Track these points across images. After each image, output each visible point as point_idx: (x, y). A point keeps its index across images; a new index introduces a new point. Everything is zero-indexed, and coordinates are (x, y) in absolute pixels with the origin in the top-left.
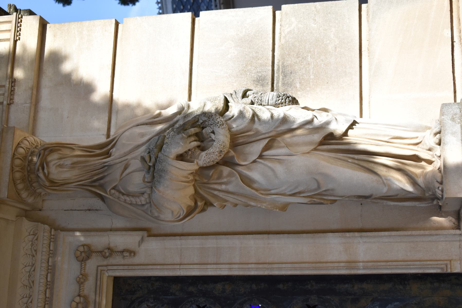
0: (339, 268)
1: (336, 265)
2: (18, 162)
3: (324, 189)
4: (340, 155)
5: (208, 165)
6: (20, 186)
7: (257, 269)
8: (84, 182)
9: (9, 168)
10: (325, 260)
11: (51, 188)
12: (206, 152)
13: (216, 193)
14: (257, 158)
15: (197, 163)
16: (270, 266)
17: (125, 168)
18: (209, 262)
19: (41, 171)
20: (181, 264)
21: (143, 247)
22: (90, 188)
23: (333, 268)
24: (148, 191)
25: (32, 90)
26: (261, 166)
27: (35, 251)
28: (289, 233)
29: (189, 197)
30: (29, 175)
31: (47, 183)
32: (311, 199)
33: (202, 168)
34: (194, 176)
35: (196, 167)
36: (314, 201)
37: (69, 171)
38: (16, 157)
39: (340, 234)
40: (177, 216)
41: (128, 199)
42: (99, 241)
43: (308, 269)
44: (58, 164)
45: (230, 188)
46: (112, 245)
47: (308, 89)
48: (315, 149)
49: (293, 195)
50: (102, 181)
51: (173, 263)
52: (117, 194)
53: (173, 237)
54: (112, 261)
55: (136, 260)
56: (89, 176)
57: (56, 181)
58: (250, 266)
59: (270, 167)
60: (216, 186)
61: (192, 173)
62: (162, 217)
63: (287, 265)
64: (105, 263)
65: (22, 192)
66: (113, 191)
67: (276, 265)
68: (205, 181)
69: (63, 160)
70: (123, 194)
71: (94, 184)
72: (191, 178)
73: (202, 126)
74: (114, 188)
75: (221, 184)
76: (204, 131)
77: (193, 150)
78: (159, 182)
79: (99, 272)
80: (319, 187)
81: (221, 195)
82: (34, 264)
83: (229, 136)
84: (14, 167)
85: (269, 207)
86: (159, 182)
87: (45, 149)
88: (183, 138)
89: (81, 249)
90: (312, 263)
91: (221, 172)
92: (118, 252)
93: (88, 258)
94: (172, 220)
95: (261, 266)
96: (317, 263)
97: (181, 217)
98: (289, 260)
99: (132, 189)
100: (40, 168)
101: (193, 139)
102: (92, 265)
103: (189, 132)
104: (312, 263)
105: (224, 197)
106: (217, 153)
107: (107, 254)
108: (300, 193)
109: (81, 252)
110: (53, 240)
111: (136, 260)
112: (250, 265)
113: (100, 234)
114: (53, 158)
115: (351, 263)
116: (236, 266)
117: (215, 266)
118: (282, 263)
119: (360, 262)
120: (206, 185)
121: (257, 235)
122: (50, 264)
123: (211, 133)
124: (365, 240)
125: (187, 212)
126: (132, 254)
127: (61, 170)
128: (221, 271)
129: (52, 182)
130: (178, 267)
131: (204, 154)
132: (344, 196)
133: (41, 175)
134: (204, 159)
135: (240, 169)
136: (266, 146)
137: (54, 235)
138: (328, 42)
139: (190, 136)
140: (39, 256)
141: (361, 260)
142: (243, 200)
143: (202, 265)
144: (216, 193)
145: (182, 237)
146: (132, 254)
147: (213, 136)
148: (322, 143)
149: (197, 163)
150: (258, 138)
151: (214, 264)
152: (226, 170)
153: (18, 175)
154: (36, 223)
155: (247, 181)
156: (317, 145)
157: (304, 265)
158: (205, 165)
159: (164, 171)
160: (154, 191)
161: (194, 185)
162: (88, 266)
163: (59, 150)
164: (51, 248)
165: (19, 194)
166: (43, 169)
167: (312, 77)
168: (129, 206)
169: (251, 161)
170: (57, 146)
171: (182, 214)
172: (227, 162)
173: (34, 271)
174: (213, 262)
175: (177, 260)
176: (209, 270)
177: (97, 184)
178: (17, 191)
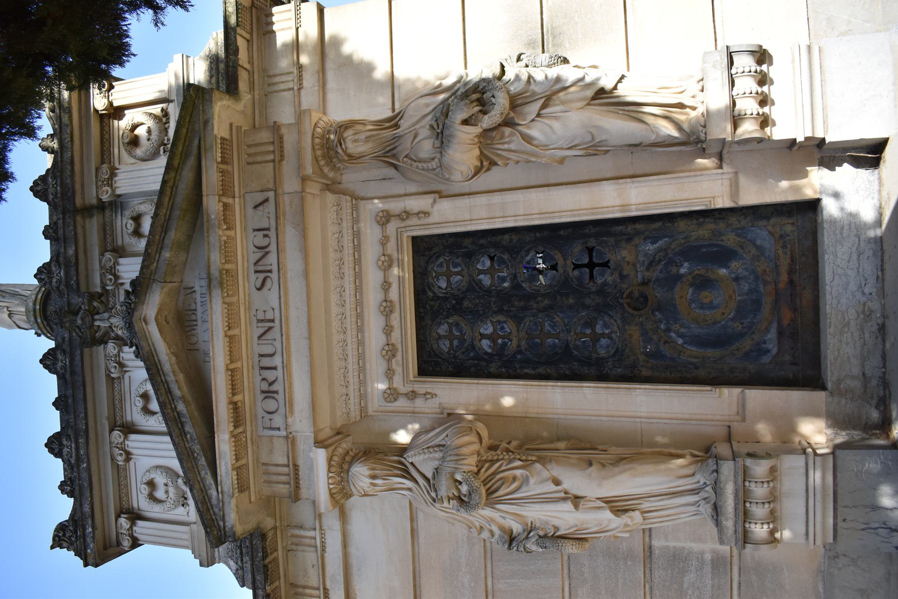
4: (611, 108)
6: (322, 163)
13: (499, 152)
17: (415, 137)
21: (436, 207)
24: (438, 155)
28: (567, 184)
33: (486, 131)
35: (480, 130)
41: (420, 165)
42: (396, 206)
43: (586, 215)
45: (512, 146)
46: (408, 209)
48: (588, 104)
50: (394, 152)
52: (409, 161)
54: (409, 222)
55: (431, 220)
59: (547, 125)
62: (453, 178)
64: (403, 225)
66: (405, 159)
68: (489, 142)
70: (415, 161)
72: (477, 140)
74: (406, 157)
75: (503, 143)
81: (504, 153)
88: (466, 104)
89: (381, 214)
91: (503, 132)
93: (388, 221)
95: (543, 216)
98: (569, 208)
99: (423, 155)
101: (475, 104)
102: (392, 228)
108: (575, 146)
110: (355, 208)
111: (431, 220)
117: (502, 219)
124: (636, 185)
131: (486, 117)
133: (340, 150)
134: (487, 121)
135: (520, 128)
139: (472, 102)
140: (344, 224)
142: (525, 156)
144: (499, 152)
147: (493, 100)
148: (594, 98)
152: (507, 131)
153: (319, 153)
155: (528, 139)
166: (341, 145)
172: (508, 123)
175: (468, 217)
177: (389, 154)
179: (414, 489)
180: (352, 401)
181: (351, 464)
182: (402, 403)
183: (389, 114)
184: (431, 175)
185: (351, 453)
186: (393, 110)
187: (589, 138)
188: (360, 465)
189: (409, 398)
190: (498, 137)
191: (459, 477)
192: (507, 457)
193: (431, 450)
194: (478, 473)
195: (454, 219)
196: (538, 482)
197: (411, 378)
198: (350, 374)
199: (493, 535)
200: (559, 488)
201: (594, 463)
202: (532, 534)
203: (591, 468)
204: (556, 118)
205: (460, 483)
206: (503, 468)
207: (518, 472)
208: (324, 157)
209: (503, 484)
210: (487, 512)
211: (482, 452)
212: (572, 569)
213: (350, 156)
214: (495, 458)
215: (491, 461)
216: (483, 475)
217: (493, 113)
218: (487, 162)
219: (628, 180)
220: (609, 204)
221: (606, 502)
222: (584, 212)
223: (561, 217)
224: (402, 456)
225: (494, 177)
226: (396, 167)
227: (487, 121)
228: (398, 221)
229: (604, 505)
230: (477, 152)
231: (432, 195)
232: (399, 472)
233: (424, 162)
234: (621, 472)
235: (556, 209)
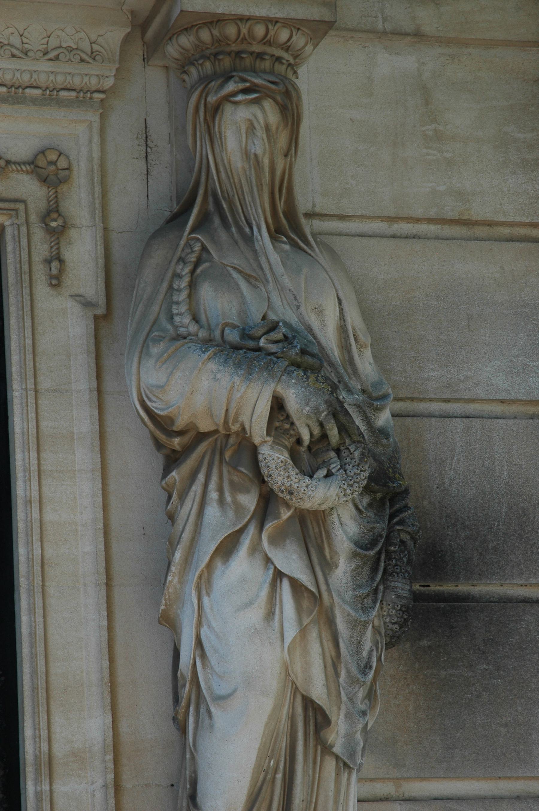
0: (37, 740)
1: (44, 733)
2: (260, 30)
3: (213, 709)
4: (284, 743)
5: (262, 464)
6: (205, 35)
7: (30, 560)
8: (215, 178)
9: (247, 13)
10: (54, 708)
11: (202, 106)
12: (290, 461)
13: (201, 477)
14: (275, 568)
15: (266, 442)
16: (38, 590)
17: (247, 278)
18: (43, 455)
19: (241, 86)
20: (36, 391)
21: (70, 304)
22: (201, 191)
23: (36, 727)
24: (203, 334)
25: (415, 35)
26: (262, 577)
27: (57, 58)
28: (110, 629)
29: (191, 422)
30: (229, 54)
31: (215, 98)
32: (189, 678)
33: (254, 450)
34: (237, 433)
35: (257, 440)
36: (184, 686)
37: (241, 146)
38: (270, 27)
39: (110, 741)
40: (151, 396)
41: (184, 283)
42: (78, 202)
43: (34, 673)
44: (256, 124)
45: (212, 511)
46: (73, 233)
47: (417, 665)
48: (296, 690)
49: (199, 643)
50: (217, 221)
51: (38, 372)
52: (193, 258)
53: (95, 374)
54: (38, 234)
55: (42, 290)
56: (229, 189)
57: (217, 122)
58: (37, 545)
59: (257, 596)
60: (214, 479)
61: (244, 429)
62: (149, 364)
63: (42, 626)
64: (33, 218)
65: (192, 38)
66: (197, 247)
67: (41, 601)
68: (227, 455)
69: (265, 136)
70: (193, 272)
71: (211, 199)
72: (235, 428)
73: (342, 448)
74: (204, 249)
75: (220, 490)
76: (333, 454)
77: (292, 432)
78: (225, 362)
79: (12, 206)
80: (220, 699)
81: (197, 488)
82: (26, 54)
83: (323, 507)
84: (249, 22)
85: (170, 590)
86: (225, 362)
87: (287, 93)
88: (317, 411)
89: (62, 163)
90: (47, 682)
91: (247, 491)
92: (58, 249)
93: (44, 180)
94: (142, 384)
95: (37, 568)
96: (47, 692)
97: (149, 403)
98: (51, 631)
99: (207, 293)
100: (248, 84)
101: (317, 431)
102: (27, 187)
103: (331, 425)
104: (47, 682)
105: (191, 494)
106: (288, 484)
107: (53, 224)
108: (203, 656)
109: (54, 163)
110: (83, 97)
111: (42, 290)
112: (39, 544)
113: (97, 206)
114: (269, 113)
115: (48, 766)
116: (36, 514)
117: (34, 468)
118: (44, 617)
119: (51, 785)
120: (217, 457)
121: (103, 559)
122: (28, 91)
123: (329, 471)
124: (99, 795)
125: (159, 415)
126: (54, 282)
127: (243, 130)
128: (25, 482)
129: (216, 110)
130: (31, 385)
131: (285, 456)
132: (195, 749)
133: (231, 87)
134: (274, 458)
135: (252, 530)
136: (302, 585)
137: (91, 98)
138: (520, 708)
139: (321, 425)
140: (44, 66)
141: (54, 787)
142: (186, 536)
143: (35, 440)
144: (201, 477)
145: (96, 393)
146: (54, 282)
147: (322, 472)
148: (308, 703)
149: (266, 442)
150: (318, 569)
151: (39, 465)
152: (249, 501)
153: (231, 31)
154: (117, 58)
155: (227, 549)
156: (305, 694)
157: (41, 662)
158: (260, 457)
159: (250, 374)
160: (207, 350)
161: (216, 431)
162: (26, 178)
163: (286, 125)
164: (63, 94)
165: (186, 29)
166: (245, 91)
167: (443, 673)
168: (165, 285)
169: (270, 555)
170: (293, 119)
171: (154, 405)
172: (268, 501)
173: (13, 55)
174: (42, 462)
175: (45, 383)
176: (26, 454)
177: (211, 207)
178: (193, 26)
183: (303, 205)
184: (155, 308)
186: (309, 215)
187: (222, 688)
190: (235, 478)
195: (40, 349)
204: (270, 615)
208: (216, 41)
213: (217, 109)
217: (293, 472)
218: (176, 445)
219: (111, 776)
220: (56, 728)
222: (41, 668)
223: (32, 611)
225: (135, 457)
226: (177, 218)
227: (274, 458)
228: (43, 205)
230: (205, 426)
231: (102, 300)
233: (190, 296)
235: (52, 601)
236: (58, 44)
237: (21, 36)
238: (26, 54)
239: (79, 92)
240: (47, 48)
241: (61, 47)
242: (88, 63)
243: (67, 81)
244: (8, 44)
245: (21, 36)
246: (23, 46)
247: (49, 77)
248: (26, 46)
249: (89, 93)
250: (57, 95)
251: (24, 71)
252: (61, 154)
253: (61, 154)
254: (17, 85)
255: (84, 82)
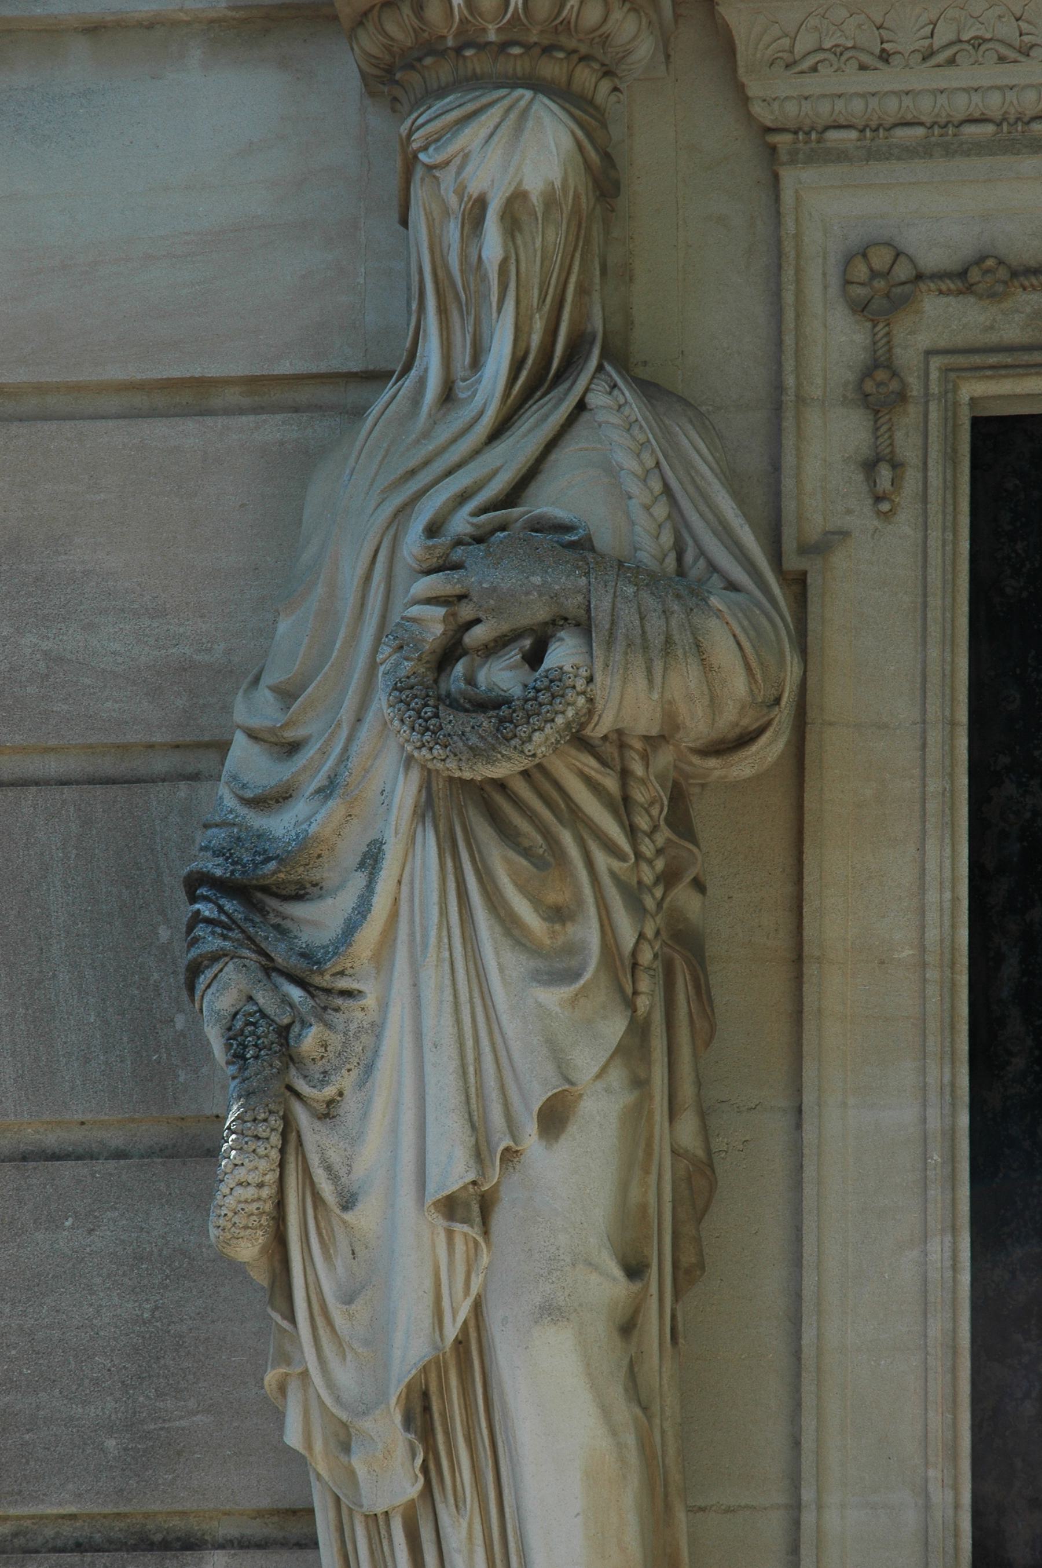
122: (832, 135)
179: (463, 415)
180: (856, 82)
181: (564, 94)
182: (835, 341)
185: (605, 86)
188: (567, 143)
189: (867, 373)
191: (563, 653)
192: (648, 876)
193: (661, 510)
194: (580, 741)
196: (555, 1026)
197: (972, 389)
198: (989, 74)
199: (261, 802)
200: (531, 1129)
201: (636, 1287)
202: (296, 993)
203: (618, 1272)
205: (534, 658)
206: (602, 860)
207: (588, 933)
209: (526, 853)
210: (406, 792)
211: (664, 758)
212: (67, 1170)
214: (643, 823)
215: (626, 799)
216: (571, 772)
221: (461, 1343)
224: (604, 354)
229: (451, 1332)
232: (536, 339)
234: (606, 1412)
236: (952, 37)
237: (1017, 20)
238: (1028, 55)
239: (796, 133)
240: (931, 45)
241: (960, 41)
242: (1016, 61)
243: (836, 112)
244: (854, 47)
245: (1017, 20)
246: (1021, 41)
247: (901, 101)
248: (1025, 38)
249: (1020, 124)
250: (818, 142)
251: (786, 98)
252: (898, 255)
253: (898, 255)
254: (943, 120)
255: (938, 105)
